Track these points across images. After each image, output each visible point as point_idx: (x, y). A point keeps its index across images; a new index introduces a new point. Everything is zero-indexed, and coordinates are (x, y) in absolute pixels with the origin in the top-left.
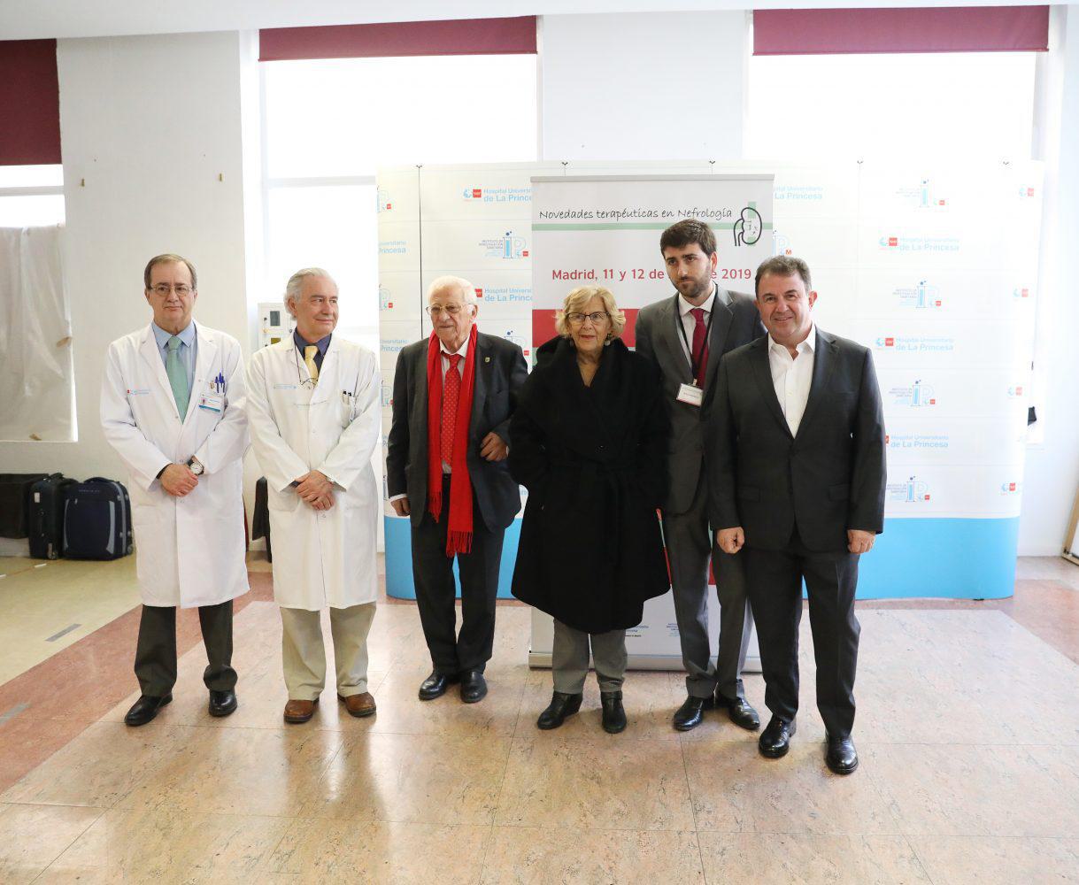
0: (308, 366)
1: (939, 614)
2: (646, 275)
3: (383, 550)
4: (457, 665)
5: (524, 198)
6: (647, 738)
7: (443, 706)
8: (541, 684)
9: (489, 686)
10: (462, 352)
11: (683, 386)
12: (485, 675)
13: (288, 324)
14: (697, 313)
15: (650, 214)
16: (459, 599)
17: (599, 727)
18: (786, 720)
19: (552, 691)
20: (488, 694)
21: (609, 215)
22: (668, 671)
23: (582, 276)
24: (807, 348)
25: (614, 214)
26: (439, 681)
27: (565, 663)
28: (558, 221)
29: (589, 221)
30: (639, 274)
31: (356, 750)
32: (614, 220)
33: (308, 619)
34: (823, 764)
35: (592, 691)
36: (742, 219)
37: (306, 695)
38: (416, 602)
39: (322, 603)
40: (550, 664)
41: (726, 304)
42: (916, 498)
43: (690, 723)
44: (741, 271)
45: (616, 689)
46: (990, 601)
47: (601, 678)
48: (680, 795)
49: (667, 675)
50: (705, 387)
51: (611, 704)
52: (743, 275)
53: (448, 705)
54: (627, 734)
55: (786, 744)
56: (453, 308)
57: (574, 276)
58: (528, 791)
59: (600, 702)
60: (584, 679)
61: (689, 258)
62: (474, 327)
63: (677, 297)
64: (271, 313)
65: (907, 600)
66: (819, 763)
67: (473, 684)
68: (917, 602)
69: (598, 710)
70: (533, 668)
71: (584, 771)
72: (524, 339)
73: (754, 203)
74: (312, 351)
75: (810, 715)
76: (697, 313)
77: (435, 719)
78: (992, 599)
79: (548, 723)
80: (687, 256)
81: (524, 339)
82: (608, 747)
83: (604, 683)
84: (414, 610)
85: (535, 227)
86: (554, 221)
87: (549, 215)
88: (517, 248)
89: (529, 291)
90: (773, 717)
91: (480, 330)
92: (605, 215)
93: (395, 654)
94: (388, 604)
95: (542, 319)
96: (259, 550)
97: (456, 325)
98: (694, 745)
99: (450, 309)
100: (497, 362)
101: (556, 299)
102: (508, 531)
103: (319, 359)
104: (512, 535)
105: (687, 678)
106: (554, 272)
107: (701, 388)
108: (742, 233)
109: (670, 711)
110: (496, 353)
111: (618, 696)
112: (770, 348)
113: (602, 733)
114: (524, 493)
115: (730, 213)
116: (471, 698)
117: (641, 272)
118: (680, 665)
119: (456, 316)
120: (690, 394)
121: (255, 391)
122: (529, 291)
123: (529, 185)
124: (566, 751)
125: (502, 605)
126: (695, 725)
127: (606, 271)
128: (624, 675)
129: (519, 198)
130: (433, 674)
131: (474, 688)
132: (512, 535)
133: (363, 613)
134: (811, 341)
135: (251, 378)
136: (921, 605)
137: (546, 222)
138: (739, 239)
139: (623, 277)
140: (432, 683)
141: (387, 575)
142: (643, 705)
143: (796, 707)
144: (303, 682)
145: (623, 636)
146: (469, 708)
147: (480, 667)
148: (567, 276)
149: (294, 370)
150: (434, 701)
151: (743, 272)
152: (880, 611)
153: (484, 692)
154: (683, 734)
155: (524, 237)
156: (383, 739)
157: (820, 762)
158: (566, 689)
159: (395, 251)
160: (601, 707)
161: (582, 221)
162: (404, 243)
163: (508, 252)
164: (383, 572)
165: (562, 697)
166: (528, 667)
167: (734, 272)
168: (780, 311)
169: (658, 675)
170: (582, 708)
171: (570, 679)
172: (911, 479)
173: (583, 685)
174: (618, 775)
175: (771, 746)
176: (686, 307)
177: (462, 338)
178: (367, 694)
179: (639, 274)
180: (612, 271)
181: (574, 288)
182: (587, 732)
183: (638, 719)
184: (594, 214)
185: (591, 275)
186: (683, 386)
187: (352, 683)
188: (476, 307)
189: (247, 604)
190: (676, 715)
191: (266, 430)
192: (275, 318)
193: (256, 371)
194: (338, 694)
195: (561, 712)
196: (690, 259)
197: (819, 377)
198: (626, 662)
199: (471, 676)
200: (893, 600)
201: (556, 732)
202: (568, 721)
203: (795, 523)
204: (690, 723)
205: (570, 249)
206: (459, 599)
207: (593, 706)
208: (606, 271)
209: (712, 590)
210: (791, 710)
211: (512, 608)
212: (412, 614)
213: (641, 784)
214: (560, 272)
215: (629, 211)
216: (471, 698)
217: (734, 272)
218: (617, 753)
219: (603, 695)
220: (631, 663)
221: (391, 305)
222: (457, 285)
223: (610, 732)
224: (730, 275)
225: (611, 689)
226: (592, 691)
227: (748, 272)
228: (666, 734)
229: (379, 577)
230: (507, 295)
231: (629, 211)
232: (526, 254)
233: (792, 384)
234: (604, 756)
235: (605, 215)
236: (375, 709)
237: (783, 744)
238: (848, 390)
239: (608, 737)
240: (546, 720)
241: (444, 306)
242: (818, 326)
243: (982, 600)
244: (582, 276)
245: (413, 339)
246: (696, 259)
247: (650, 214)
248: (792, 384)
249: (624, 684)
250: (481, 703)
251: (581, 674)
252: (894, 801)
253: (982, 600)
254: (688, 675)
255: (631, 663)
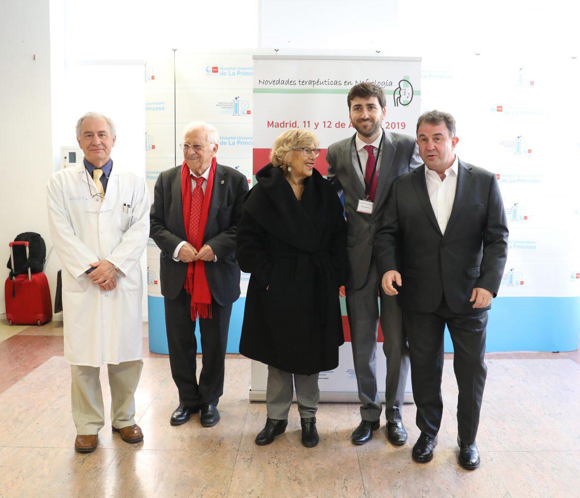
0: (98, 185)
1: (530, 362)
2: (333, 125)
3: (147, 320)
4: (198, 400)
5: (248, 74)
6: (334, 450)
7: (188, 429)
8: (258, 413)
9: (221, 414)
10: (205, 175)
11: (360, 201)
12: (218, 407)
13: (81, 155)
14: (369, 149)
15: (336, 83)
16: (200, 354)
17: (299, 443)
18: (431, 436)
19: (266, 418)
20: (220, 421)
21: (307, 83)
22: (348, 403)
23: (288, 125)
24: (452, 172)
25: (310, 82)
26: (184, 411)
27: (276, 397)
28: (272, 86)
29: (293, 87)
30: (328, 125)
31: (126, 466)
32: (311, 87)
33: (91, 373)
34: (457, 466)
35: (294, 419)
36: (400, 87)
37: (91, 431)
38: (169, 356)
39: (103, 358)
40: (265, 399)
41: (392, 142)
42: (514, 282)
43: (364, 439)
44: (398, 123)
45: (312, 416)
46: (563, 353)
47: (301, 408)
48: (358, 491)
49: (346, 406)
50: (375, 201)
51: (308, 426)
52: (400, 127)
53: (191, 430)
54: (319, 447)
55: (431, 452)
56: (197, 146)
57: (282, 125)
58: (249, 490)
59: (300, 425)
60: (288, 409)
61: (371, 107)
62: (214, 160)
63: (354, 137)
64: (70, 153)
65: (508, 353)
66: (454, 467)
67: (209, 413)
68: (497, 355)
69: (299, 431)
70: (253, 402)
71: (289, 475)
72: (247, 170)
73: (408, 77)
74: (99, 173)
75: (447, 432)
76: (369, 149)
77: (182, 439)
78: (565, 352)
79: (263, 441)
80: (370, 105)
81: (247, 170)
82: (306, 458)
83: (302, 412)
84: (167, 361)
85: (255, 91)
86: (268, 86)
87: (266, 82)
88: (243, 108)
89: (251, 138)
90: (422, 433)
91: (220, 162)
92: (304, 83)
93: (154, 395)
94: (150, 357)
95: (259, 154)
96: (58, 320)
97: (200, 157)
98: (366, 455)
99: (196, 147)
100: (230, 184)
101: (269, 140)
102: (234, 304)
103: (104, 180)
104: (238, 310)
105: (361, 407)
106: (268, 122)
107: (372, 201)
108: (400, 97)
109: (348, 431)
110: (228, 178)
111: (313, 421)
112: (426, 172)
113: (302, 447)
114: (245, 279)
115: (391, 84)
116: (208, 423)
117: (329, 123)
118: (357, 399)
119: (201, 152)
120: (365, 206)
121: (55, 202)
122: (251, 138)
123: (251, 63)
124: (276, 461)
125: (231, 358)
126: (367, 440)
127: (305, 122)
128: (317, 406)
129: (245, 74)
130: (180, 404)
131: (210, 417)
132: (238, 310)
133: (136, 366)
134: (455, 167)
135: (51, 191)
136: (518, 356)
137: (264, 87)
138: (397, 102)
139: (317, 126)
140: (179, 413)
141: (149, 337)
142: (331, 427)
143: (438, 426)
144: (88, 421)
145: (317, 379)
146: (206, 430)
147: (215, 402)
148: (278, 125)
149: (86, 187)
150: (181, 426)
151: (400, 125)
152: (490, 360)
153: (217, 419)
154: (359, 447)
155: (248, 100)
156: (145, 460)
157: (455, 465)
158: (276, 417)
159: (157, 108)
160: (301, 428)
161: (288, 87)
162: (163, 103)
163: (236, 111)
164: (147, 336)
165: (273, 422)
166: (249, 401)
167: (393, 127)
168: (429, 149)
169: (340, 406)
170: (288, 429)
171: (279, 409)
172: (511, 270)
173: (288, 412)
174: (313, 477)
175: (421, 454)
176: (361, 144)
177: (204, 166)
178: (135, 425)
179: (328, 125)
180: (309, 122)
181: (281, 133)
182: (291, 447)
183: (327, 437)
184: (297, 82)
185: (294, 125)
186: (360, 201)
187: (126, 419)
188: (217, 145)
189: (49, 358)
190: (354, 434)
191: (66, 231)
192: (73, 157)
193: (55, 186)
194: (113, 427)
195: (272, 432)
196: (371, 108)
197: (461, 188)
198: (318, 396)
199: (208, 407)
200: (499, 353)
201: (269, 447)
202: (277, 439)
203: (444, 297)
204: (364, 439)
205: (281, 106)
206: (200, 354)
207: (295, 428)
208: (305, 122)
209: (380, 346)
210: (434, 428)
211: (237, 360)
212: (165, 364)
213: (329, 484)
214: (273, 122)
215: (321, 80)
216: (208, 423)
217: (393, 127)
218: (313, 462)
219: (302, 420)
220: (322, 397)
221: (153, 147)
222: (203, 129)
223: (306, 446)
224: (397, 121)
225: (308, 416)
226: (294, 419)
227: (403, 125)
228: (347, 447)
229: (144, 339)
230: (236, 141)
231: (321, 80)
232: (249, 112)
233: (442, 198)
234: (303, 463)
235: (304, 83)
236: (142, 437)
237: (429, 452)
238: (479, 202)
239: (306, 450)
240: (262, 438)
241: (193, 145)
242: (460, 159)
243: (558, 352)
244: (288, 125)
245: (168, 165)
246: (375, 108)
247: (336, 83)
248: (442, 198)
249: (317, 413)
250: (214, 427)
251: (288, 405)
252: (508, 492)
253: (558, 352)
254: (362, 405)
255: (322, 397)
